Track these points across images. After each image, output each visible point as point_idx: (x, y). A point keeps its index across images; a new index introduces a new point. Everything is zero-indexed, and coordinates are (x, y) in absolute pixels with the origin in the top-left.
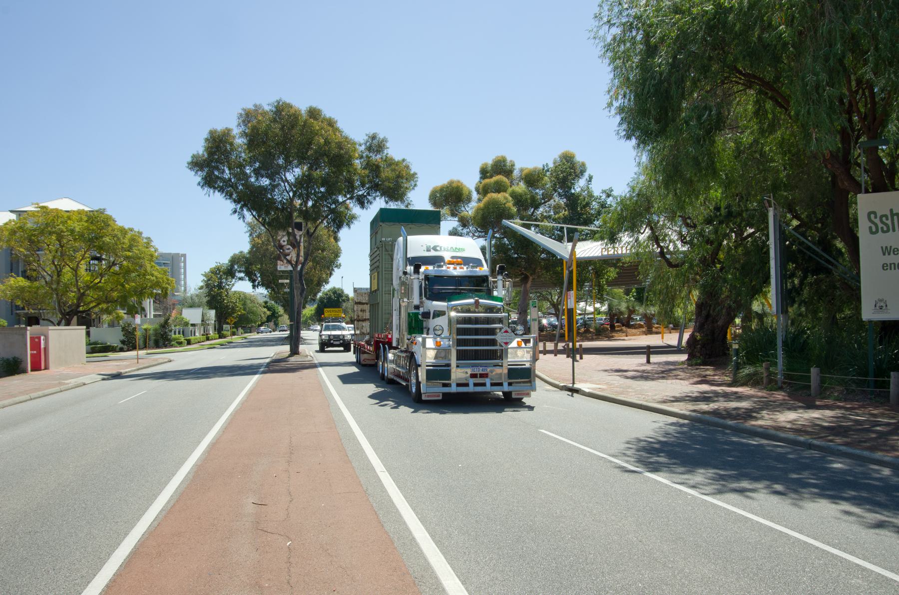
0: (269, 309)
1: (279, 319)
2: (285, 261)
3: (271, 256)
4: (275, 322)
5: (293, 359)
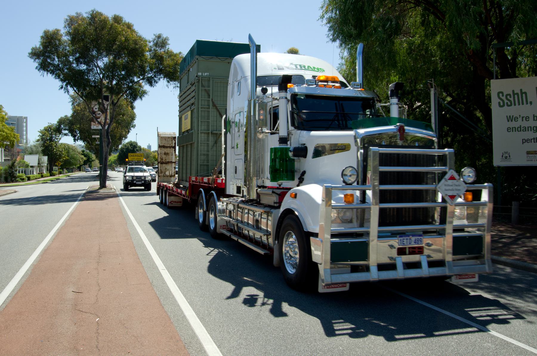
0: (85, 156)
1: (93, 163)
2: (97, 123)
3: (87, 118)
4: (89, 165)
5: (102, 191)
